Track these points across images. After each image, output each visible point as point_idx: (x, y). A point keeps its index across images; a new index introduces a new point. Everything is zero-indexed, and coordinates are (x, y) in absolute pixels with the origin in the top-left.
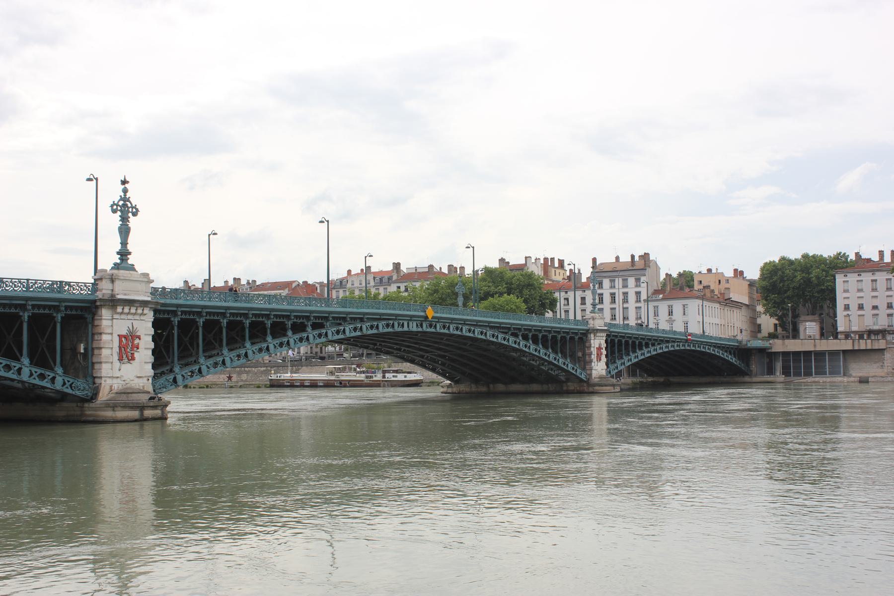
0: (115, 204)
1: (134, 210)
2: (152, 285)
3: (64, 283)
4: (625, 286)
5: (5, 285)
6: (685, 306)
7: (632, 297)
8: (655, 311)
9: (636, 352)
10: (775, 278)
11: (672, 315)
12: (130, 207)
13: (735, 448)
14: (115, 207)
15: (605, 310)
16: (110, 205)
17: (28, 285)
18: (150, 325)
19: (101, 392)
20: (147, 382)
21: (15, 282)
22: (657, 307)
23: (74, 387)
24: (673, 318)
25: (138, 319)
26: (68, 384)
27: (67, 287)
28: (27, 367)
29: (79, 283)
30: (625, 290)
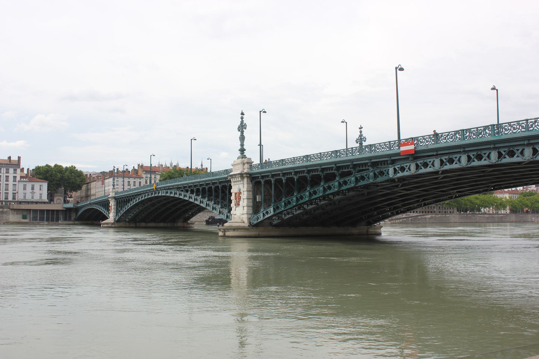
4: (7, 172)
6: (41, 186)
7: (11, 179)
8: (32, 187)
10: (48, 175)
11: (33, 190)
17: (527, 125)
22: (26, 185)
24: (34, 191)
30: (7, 175)
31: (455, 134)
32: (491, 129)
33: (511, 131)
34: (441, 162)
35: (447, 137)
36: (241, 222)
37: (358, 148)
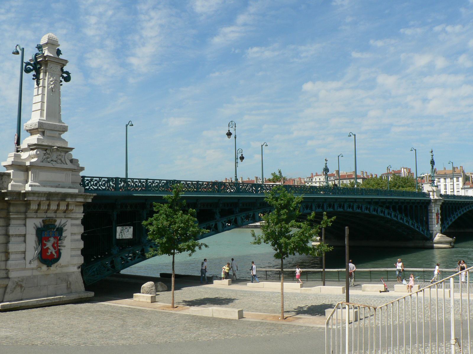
2: (82, 174)
3: (120, 179)
9: (454, 214)
13: (301, 326)
15: (456, 189)
21: (136, 182)
27: (123, 183)
29: (187, 181)
34: (83, 211)
35: (98, 184)
37: (204, 183)
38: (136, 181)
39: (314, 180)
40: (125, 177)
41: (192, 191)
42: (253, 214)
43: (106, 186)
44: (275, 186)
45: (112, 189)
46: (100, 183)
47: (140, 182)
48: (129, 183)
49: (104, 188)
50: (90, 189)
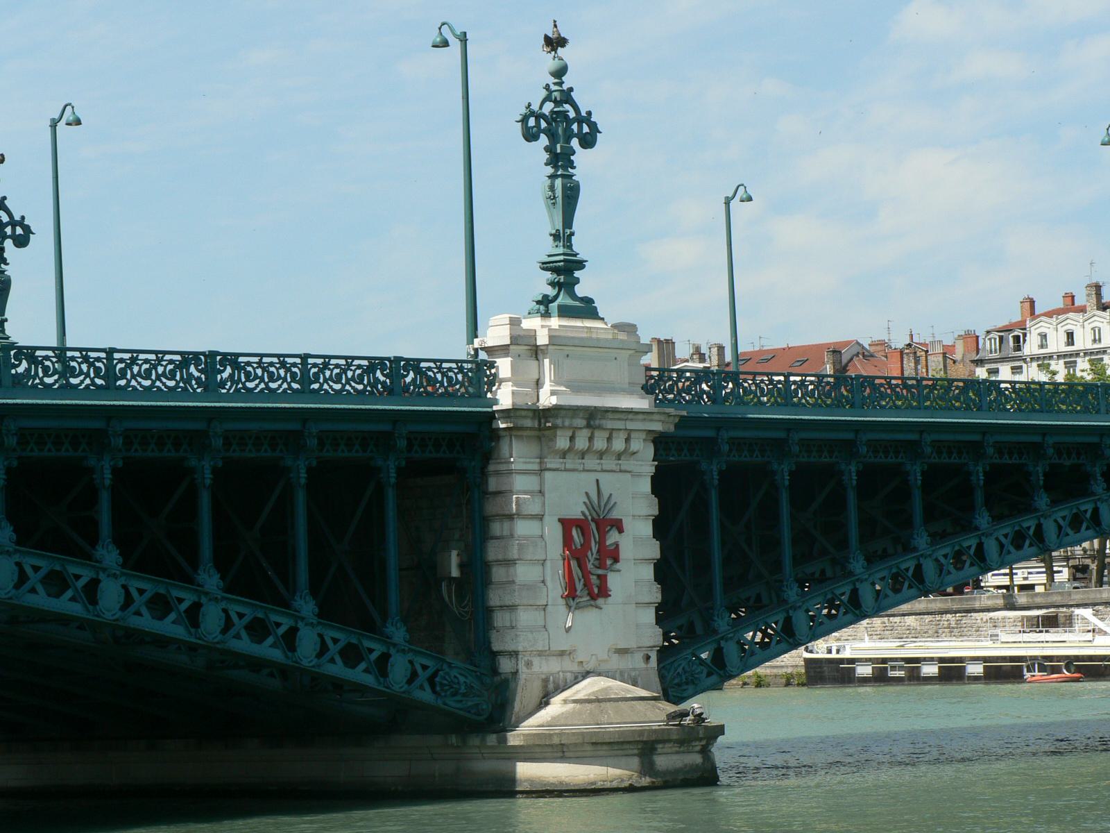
0: (532, 113)
1: (19, 231)
3: (218, 358)
5: (40, 370)
12: (574, 120)
14: (532, 122)
16: (520, 118)
17: (110, 367)
18: (646, 486)
19: (518, 699)
20: (643, 665)
21: (271, 364)
23: (442, 685)
25: (614, 467)
26: (423, 676)
27: (24, 364)
28: (115, 576)
29: (442, 361)
31: (370, 369)
32: (206, 363)
33: (285, 384)
35: (154, 372)
36: (631, 789)
38: (450, 367)
39: (1031, 347)
40: (56, 346)
41: (891, 408)
42: (1094, 509)
43: (178, 378)
44: (688, 374)
45: (195, 386)
46: (160, 369)
47: (283, 365)
48: (73, 364)
49: (171, 383)
50: (130, 389)
